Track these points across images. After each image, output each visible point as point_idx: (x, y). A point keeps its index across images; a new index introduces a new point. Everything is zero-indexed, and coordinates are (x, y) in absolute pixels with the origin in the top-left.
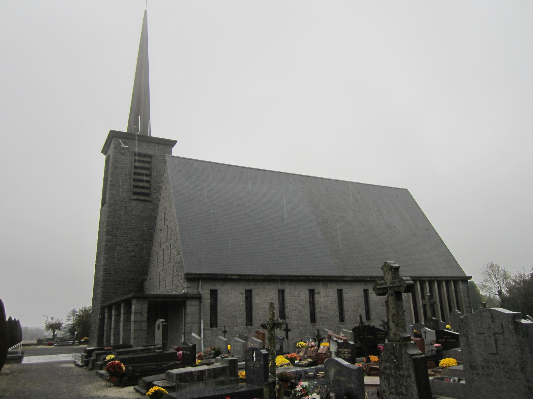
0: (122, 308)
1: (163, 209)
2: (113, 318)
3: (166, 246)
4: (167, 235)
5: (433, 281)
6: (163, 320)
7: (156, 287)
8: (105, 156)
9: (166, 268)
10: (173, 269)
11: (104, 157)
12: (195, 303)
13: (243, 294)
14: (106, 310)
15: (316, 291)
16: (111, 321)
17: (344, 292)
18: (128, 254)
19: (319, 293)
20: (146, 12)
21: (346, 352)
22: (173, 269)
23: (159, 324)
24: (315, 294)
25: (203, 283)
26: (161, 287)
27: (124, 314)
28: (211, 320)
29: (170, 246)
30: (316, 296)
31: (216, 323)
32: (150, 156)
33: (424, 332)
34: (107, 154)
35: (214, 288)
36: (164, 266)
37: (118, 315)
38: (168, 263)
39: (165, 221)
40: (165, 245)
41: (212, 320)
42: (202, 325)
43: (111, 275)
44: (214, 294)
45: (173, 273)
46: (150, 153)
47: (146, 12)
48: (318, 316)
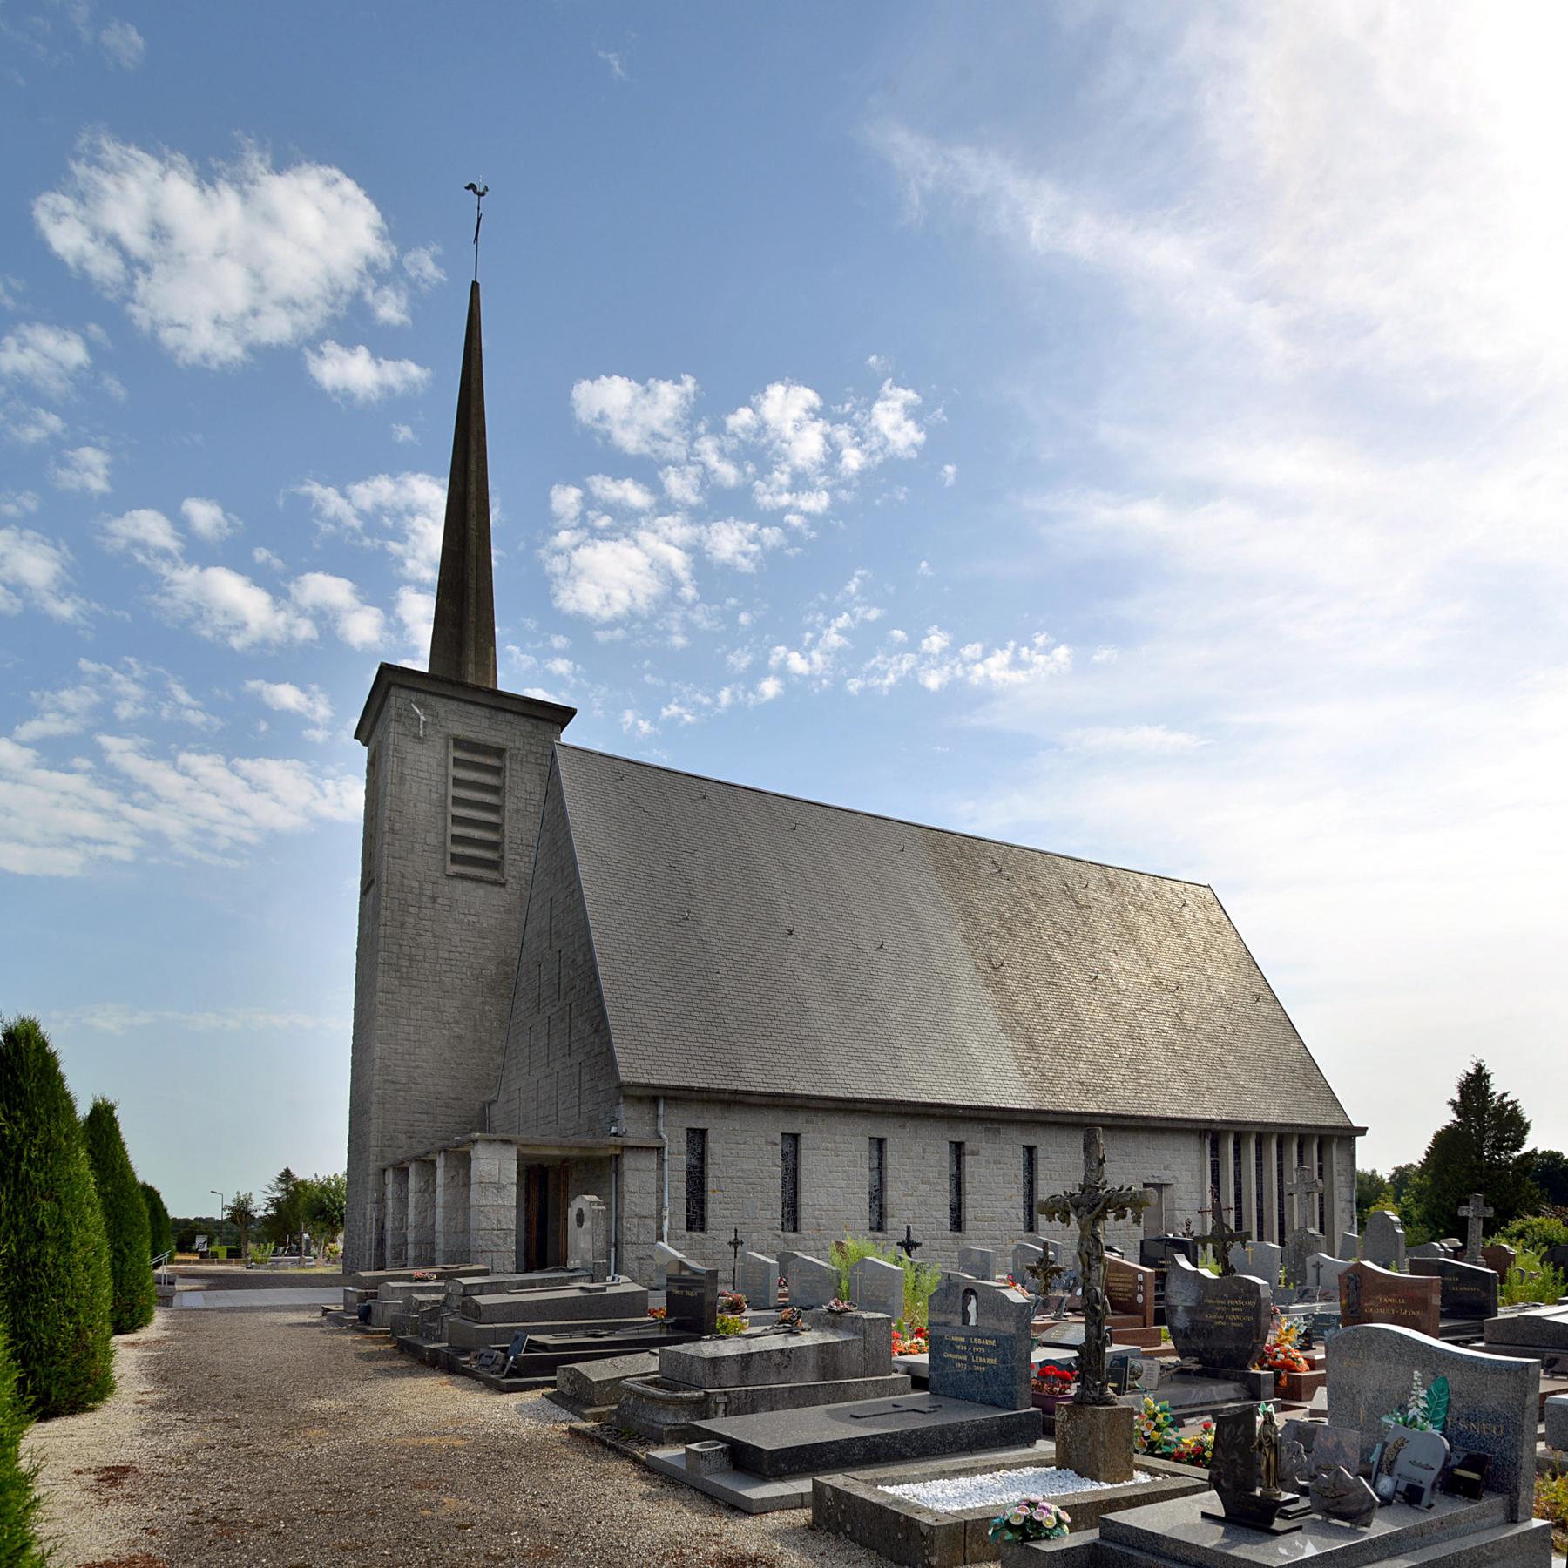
0: (440, 1173)
1: (544, 904)
2: (412, 1199)
3: (557, 1008)
4: (559, 978)
5: (1291, 1135)
6: (595, 1198)
7: (526, 1122)
8: (366, 748)
9: (556, 1070)
10: (580, 1071)
11: (142, 1176)
12: (650, 1162)
13: (776, 1144)
14: (390, 1175)
15: (968, 1147)
16: (407, 1207)
17: (1041, 1153)
18: (446, 1032)
19: (974, 1153)
20: (475, 286)
21: (1233, 1309)
22: (580, 1071)
23: (580, 1211)
24: (964, 1154)
25: (668, 1110)
26: (541, 1122)
27: (446, 1186)
28: (688, 1211)
29: (568, 1008)
30: (969, 1161)
31: (703, 1219)
32: (499, 752)
33: (1314, 1266)
34: (372, 742)
35: (699, 1124)
36: (552, 1065)
37: (429, 1187)
38: (564, 1056)
39: (550, 939)
40: (554, 1006)
41: (692, 1209)
42: (666, 1223)
43: (398, 1086)
44: (698, 1137)
45: (580, 1085)
46: (499, 740)
47: (475, 286)
48: (969, 1213)
